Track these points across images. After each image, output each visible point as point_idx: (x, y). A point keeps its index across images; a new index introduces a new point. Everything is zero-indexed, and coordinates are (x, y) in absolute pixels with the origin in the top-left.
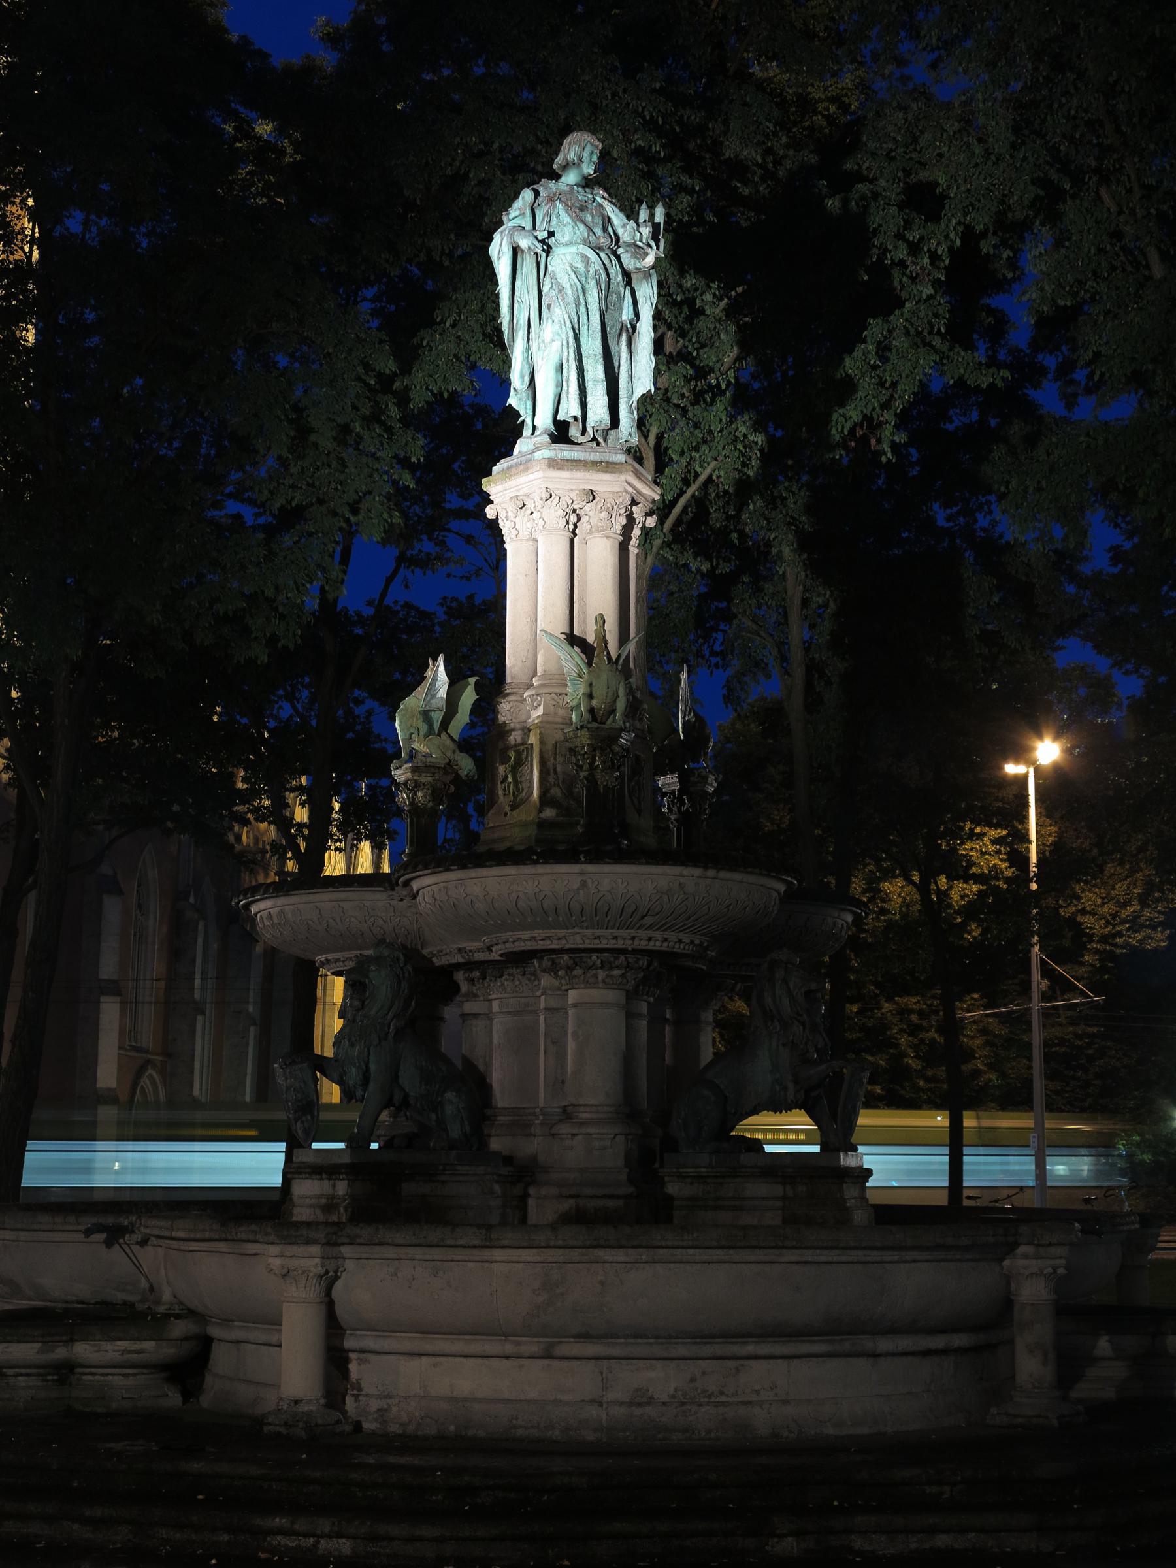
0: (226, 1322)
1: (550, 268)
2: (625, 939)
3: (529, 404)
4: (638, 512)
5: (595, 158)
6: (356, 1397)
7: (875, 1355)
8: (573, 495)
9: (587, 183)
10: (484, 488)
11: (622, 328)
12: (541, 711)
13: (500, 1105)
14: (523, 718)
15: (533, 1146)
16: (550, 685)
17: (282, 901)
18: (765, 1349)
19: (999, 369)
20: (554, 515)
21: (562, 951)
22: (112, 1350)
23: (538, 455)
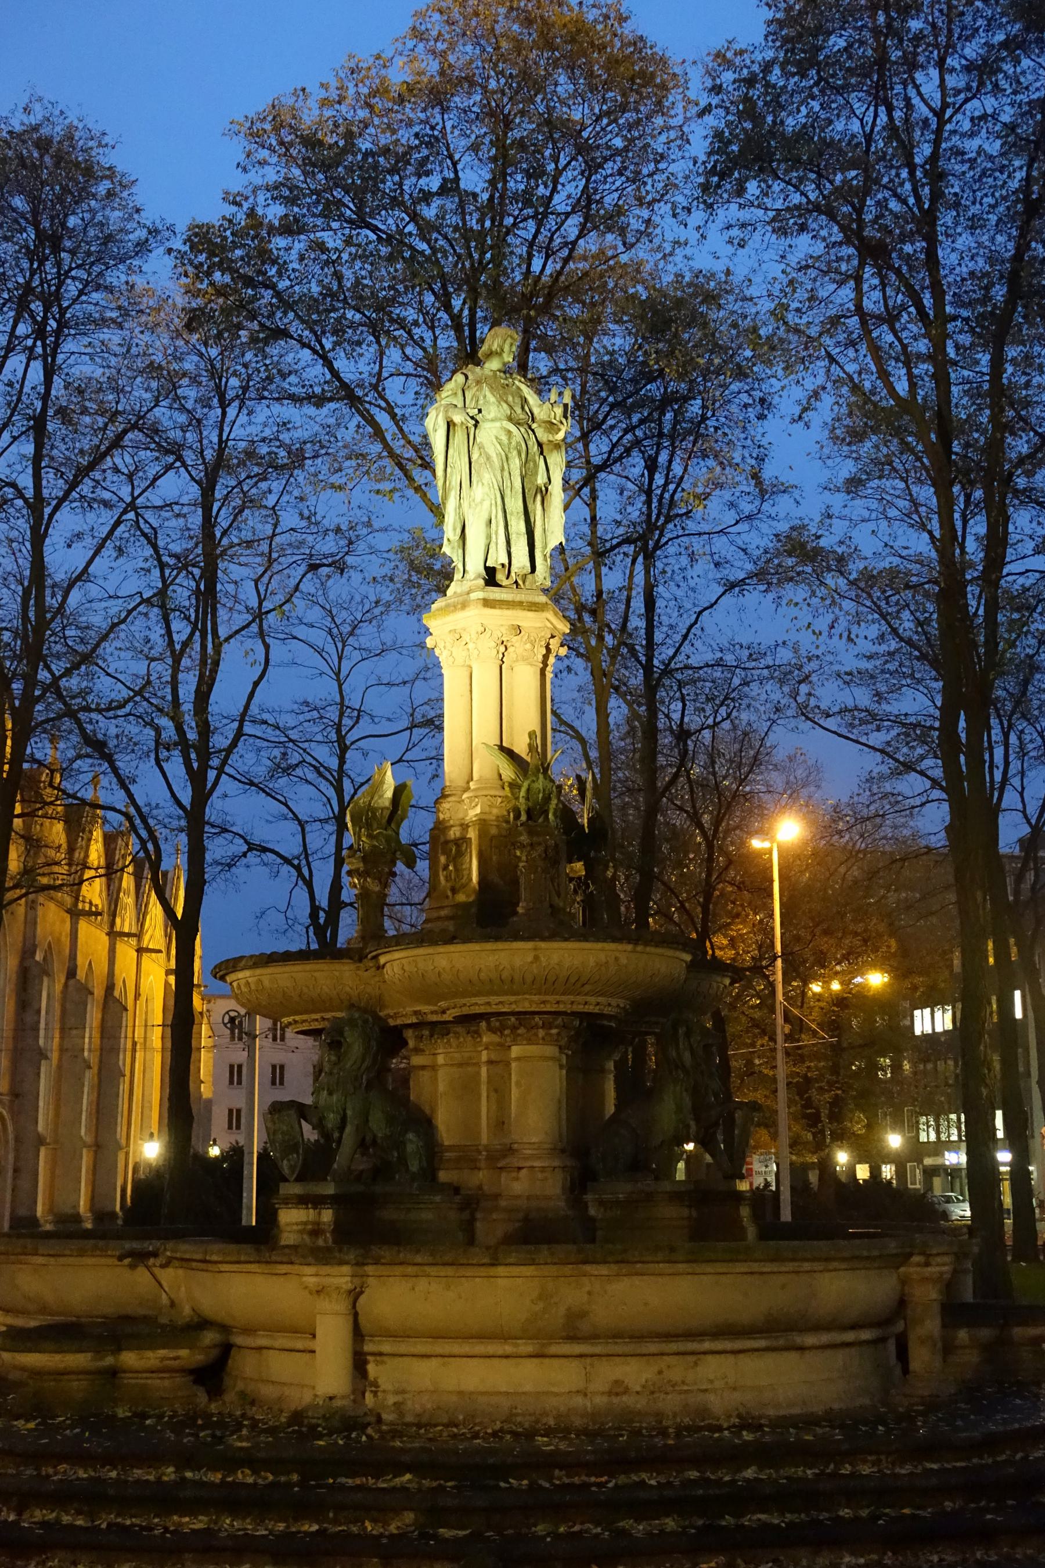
0: (249, 1330)
1: (478, 440)
2: (568, 1003)
3: (460, 551)
4: (554, 644)
5: (514, 349)
6: (375, 1393)
7: (801, 1349)
8: (504, 630)
9: (506, 371)
10: (424, 622)
11: (538, 490)
12: (478, 810)
13: (446, 1143)
14: (461, 816)
15: (480, 1178)
16: (485, 788)
17: (258, 971)
18: (719, 1345)
19: (567, 444)
20: (488, 647)
21: (513, 1013)
22: (153, 1357)
23: (474, 596)
